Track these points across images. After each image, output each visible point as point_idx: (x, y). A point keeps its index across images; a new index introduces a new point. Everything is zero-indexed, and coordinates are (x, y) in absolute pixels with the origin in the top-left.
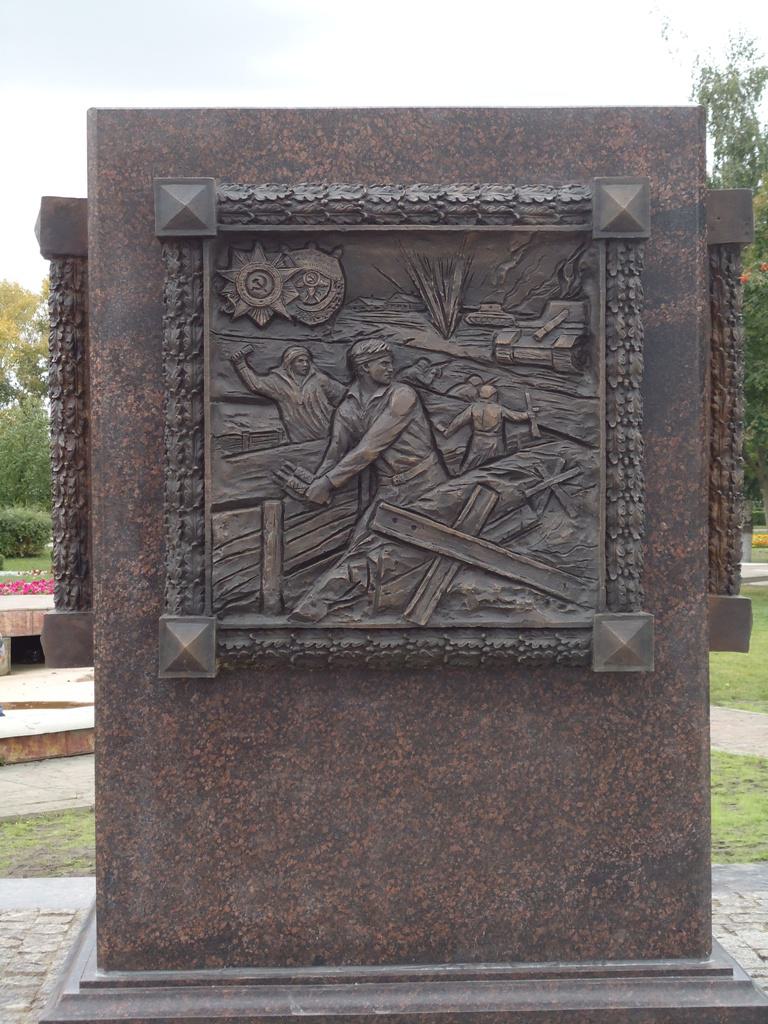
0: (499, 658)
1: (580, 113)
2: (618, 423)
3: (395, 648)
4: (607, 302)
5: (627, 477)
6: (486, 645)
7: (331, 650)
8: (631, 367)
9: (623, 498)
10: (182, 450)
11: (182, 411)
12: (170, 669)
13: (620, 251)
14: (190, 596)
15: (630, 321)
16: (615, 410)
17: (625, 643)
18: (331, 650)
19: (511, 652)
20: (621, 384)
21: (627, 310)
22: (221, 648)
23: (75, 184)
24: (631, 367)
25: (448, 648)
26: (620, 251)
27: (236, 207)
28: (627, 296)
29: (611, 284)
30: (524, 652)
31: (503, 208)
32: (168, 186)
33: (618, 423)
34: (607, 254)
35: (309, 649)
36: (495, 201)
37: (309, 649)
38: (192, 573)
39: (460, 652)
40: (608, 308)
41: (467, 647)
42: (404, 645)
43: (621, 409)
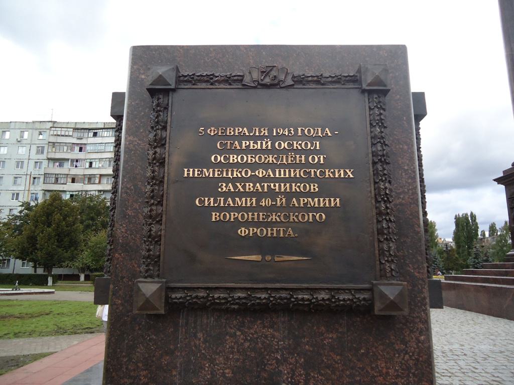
0: (321, 305)
1: (354, 46)
2: (380, 180)
3: (180, 298)
4: (370, 121)
5: (387, 208)
6: (313, 298)
7: (313, 301)
8: (385, 151)
9: (380, 142)
10: (153, 191)
11: (153, 172)
12: (141, 309)
13: (375, 97)
14: (151, 268)
15: (388, 205)
16: (378, 173)
17: (392, 298)
18: (229, 299)
19: (327, 302)
20: (380, 160)
21: (380, 124)
22: (167, 298)
23: (123, 86)
24: (390, 230)
25: (293, 300)
26: (375, 97)
27: (186, 79)
28: (386, 192)
29: (371, 113)
30: (335, 302)
31: (315, 78)
32: (382, 286)
33: (380, 180)
34: (369, 99)
35: (217, 299)
36: (312, 76)
37: (217, 299)
38: (153, 256)
39: (216, 301)
40: (371, 124)
41: (219, 298)
42: (185, 297)
43: (381, 173)
